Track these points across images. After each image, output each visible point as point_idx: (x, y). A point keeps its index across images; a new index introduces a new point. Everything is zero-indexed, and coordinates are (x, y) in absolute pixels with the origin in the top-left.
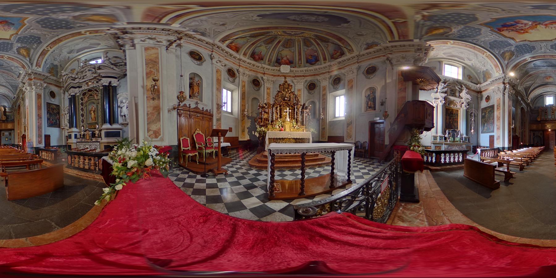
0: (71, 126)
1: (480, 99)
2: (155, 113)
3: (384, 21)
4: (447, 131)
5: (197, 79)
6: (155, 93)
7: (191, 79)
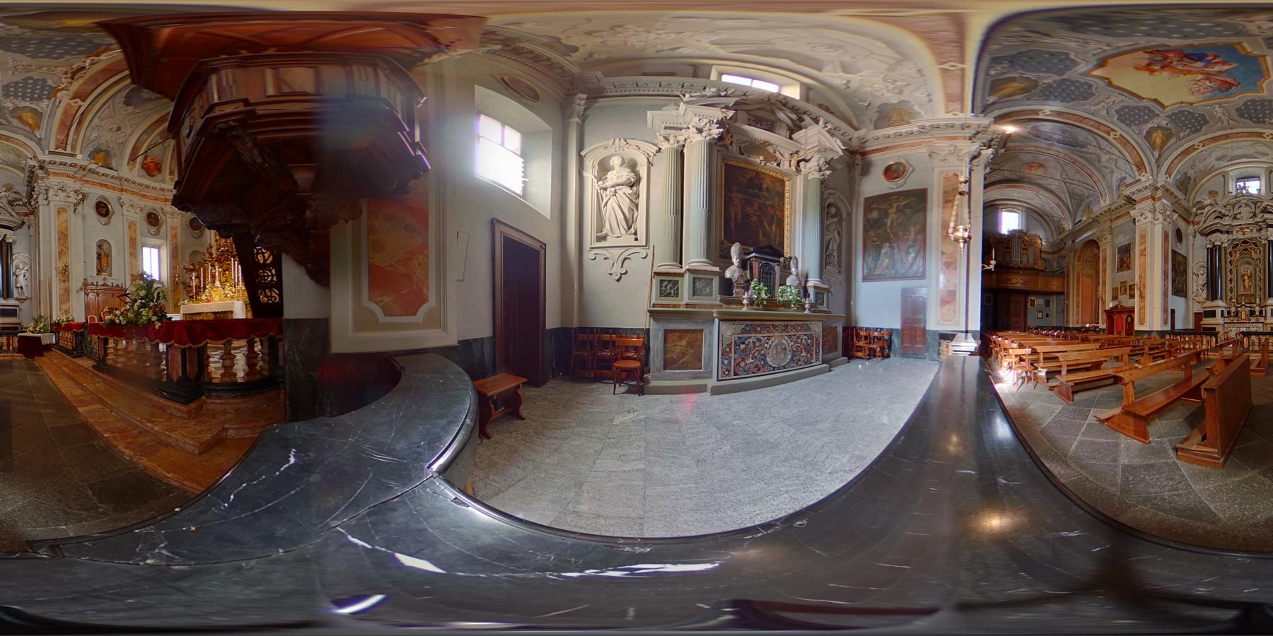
0: (1213, 295)
1: (858, 171)
2: (66, 295)
4: (735, 250)
5: (105, 246)
6: (65, 272)
7: (99, 246)
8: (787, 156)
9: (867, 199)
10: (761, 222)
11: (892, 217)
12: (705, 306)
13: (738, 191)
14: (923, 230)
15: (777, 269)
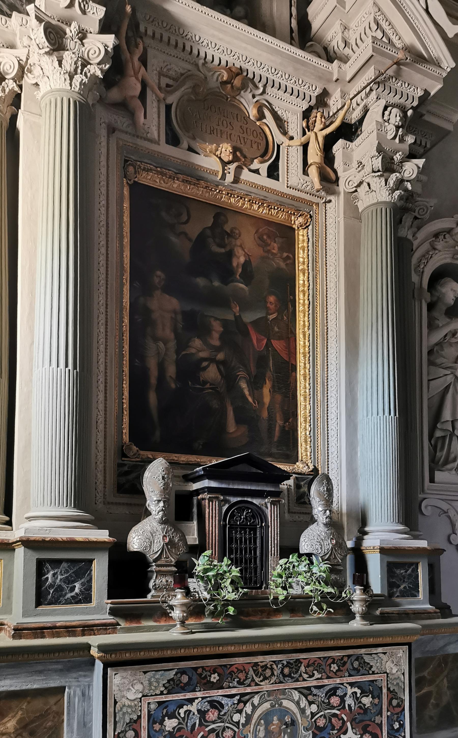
4: (154, 477)
8: (295, 124)
10: (230, 380)
12: (70, 630)
13: (168, 289)
15: (271, 513)
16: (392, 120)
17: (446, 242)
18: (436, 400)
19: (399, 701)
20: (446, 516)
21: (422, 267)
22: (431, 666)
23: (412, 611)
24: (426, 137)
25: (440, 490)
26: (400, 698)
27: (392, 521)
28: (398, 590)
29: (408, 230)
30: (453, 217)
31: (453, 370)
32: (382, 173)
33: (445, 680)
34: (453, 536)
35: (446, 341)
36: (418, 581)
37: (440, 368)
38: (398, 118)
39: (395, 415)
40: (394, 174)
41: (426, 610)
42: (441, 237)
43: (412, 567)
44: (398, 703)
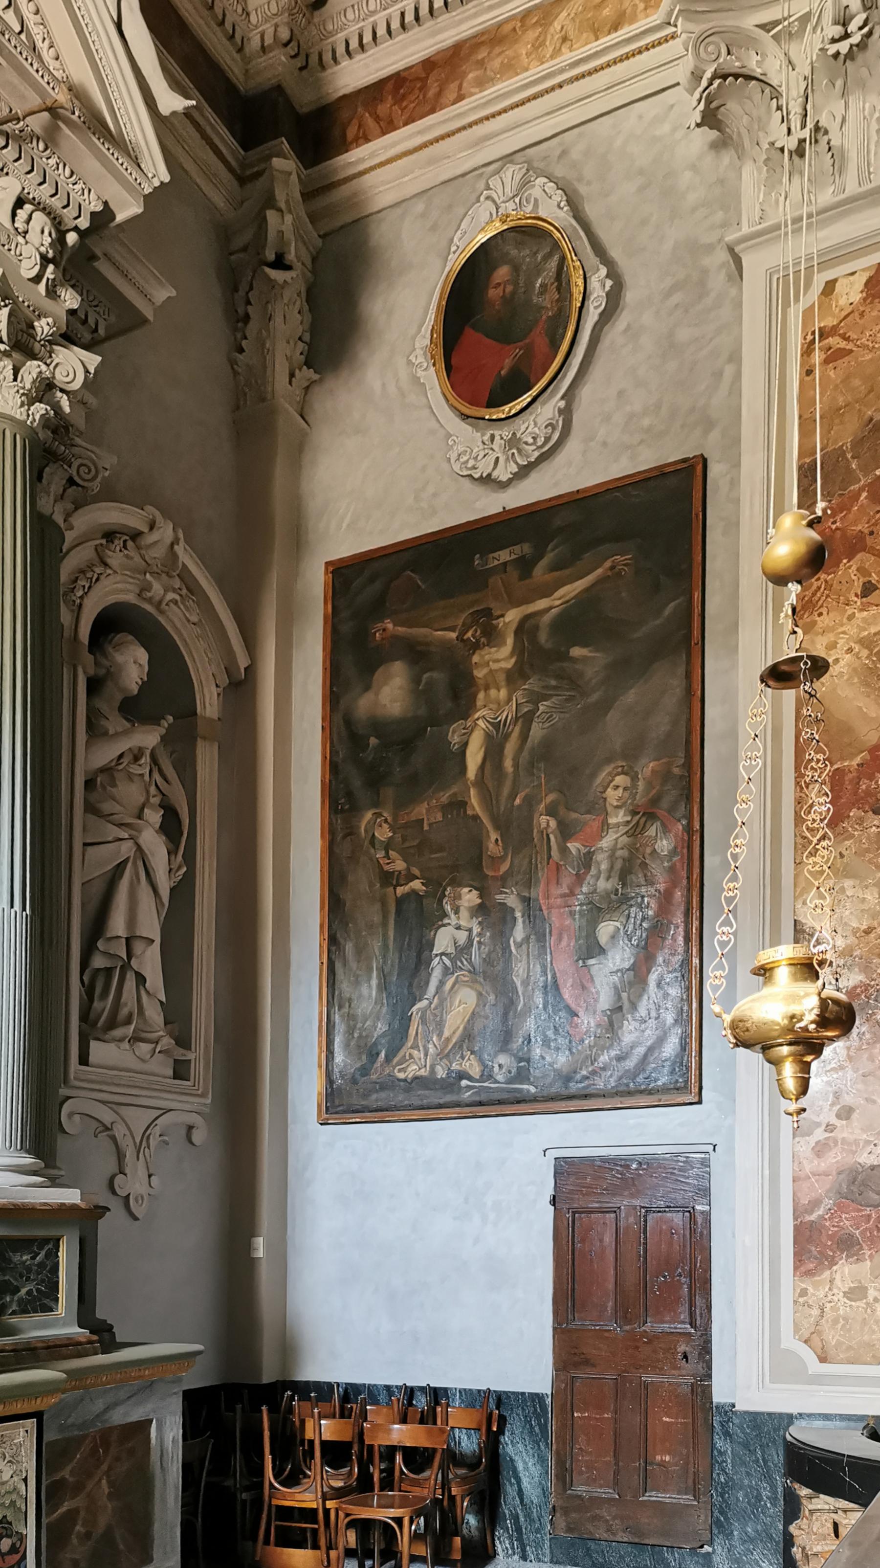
1: (286, 324)
3: (121, 1071)
9: (343, 574)
11: (494, 705)
14: (681, 789)
16: (34, 236)
17: (127, 556)
18: (97, 889)
19: (15, 1539)
20: (108, 1135)
21: (80, 593)
22: (78, 1456)
23: (43, 1341)
24: (97, 309)
25: (92, 1082)
26: (17, 1532)
27: (8, 1144)
28: (16, 1298)
29: (55, 501)
30: (142, 509)
31: (134, 833)
32: (8, 348)
33: (104, 1482)
34: (119, 1180)
35: (121, 767)
36: (58, 1277)
37: (109, 821)
38: (47, 240)
39: (24, 909)
40: (36, 363)
41: (68, 1338)
42: (118, 543)
43: (46, 1248)
44: (13, 1545)
